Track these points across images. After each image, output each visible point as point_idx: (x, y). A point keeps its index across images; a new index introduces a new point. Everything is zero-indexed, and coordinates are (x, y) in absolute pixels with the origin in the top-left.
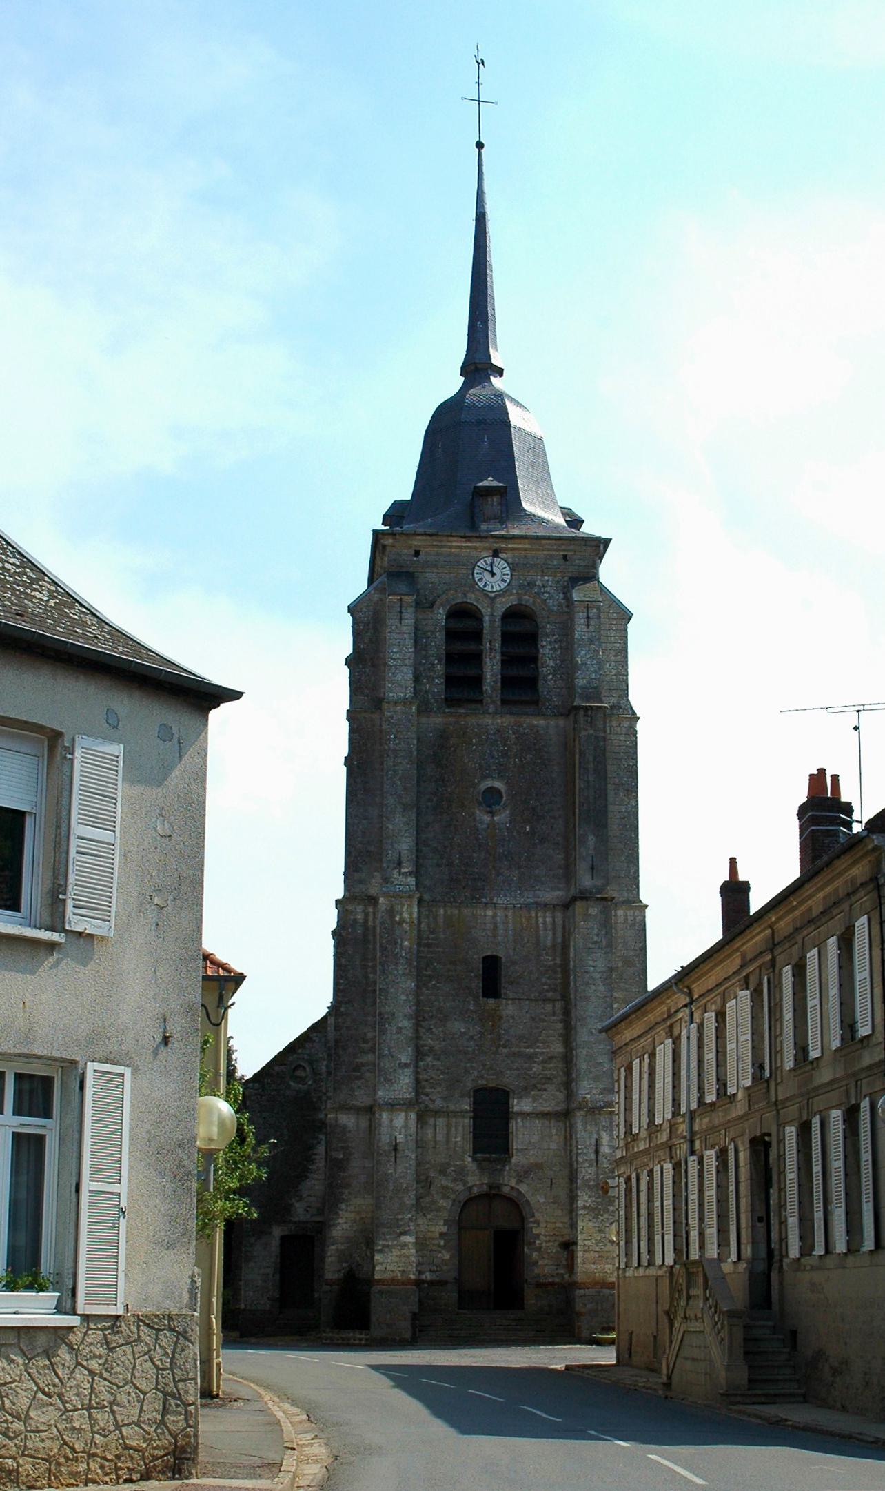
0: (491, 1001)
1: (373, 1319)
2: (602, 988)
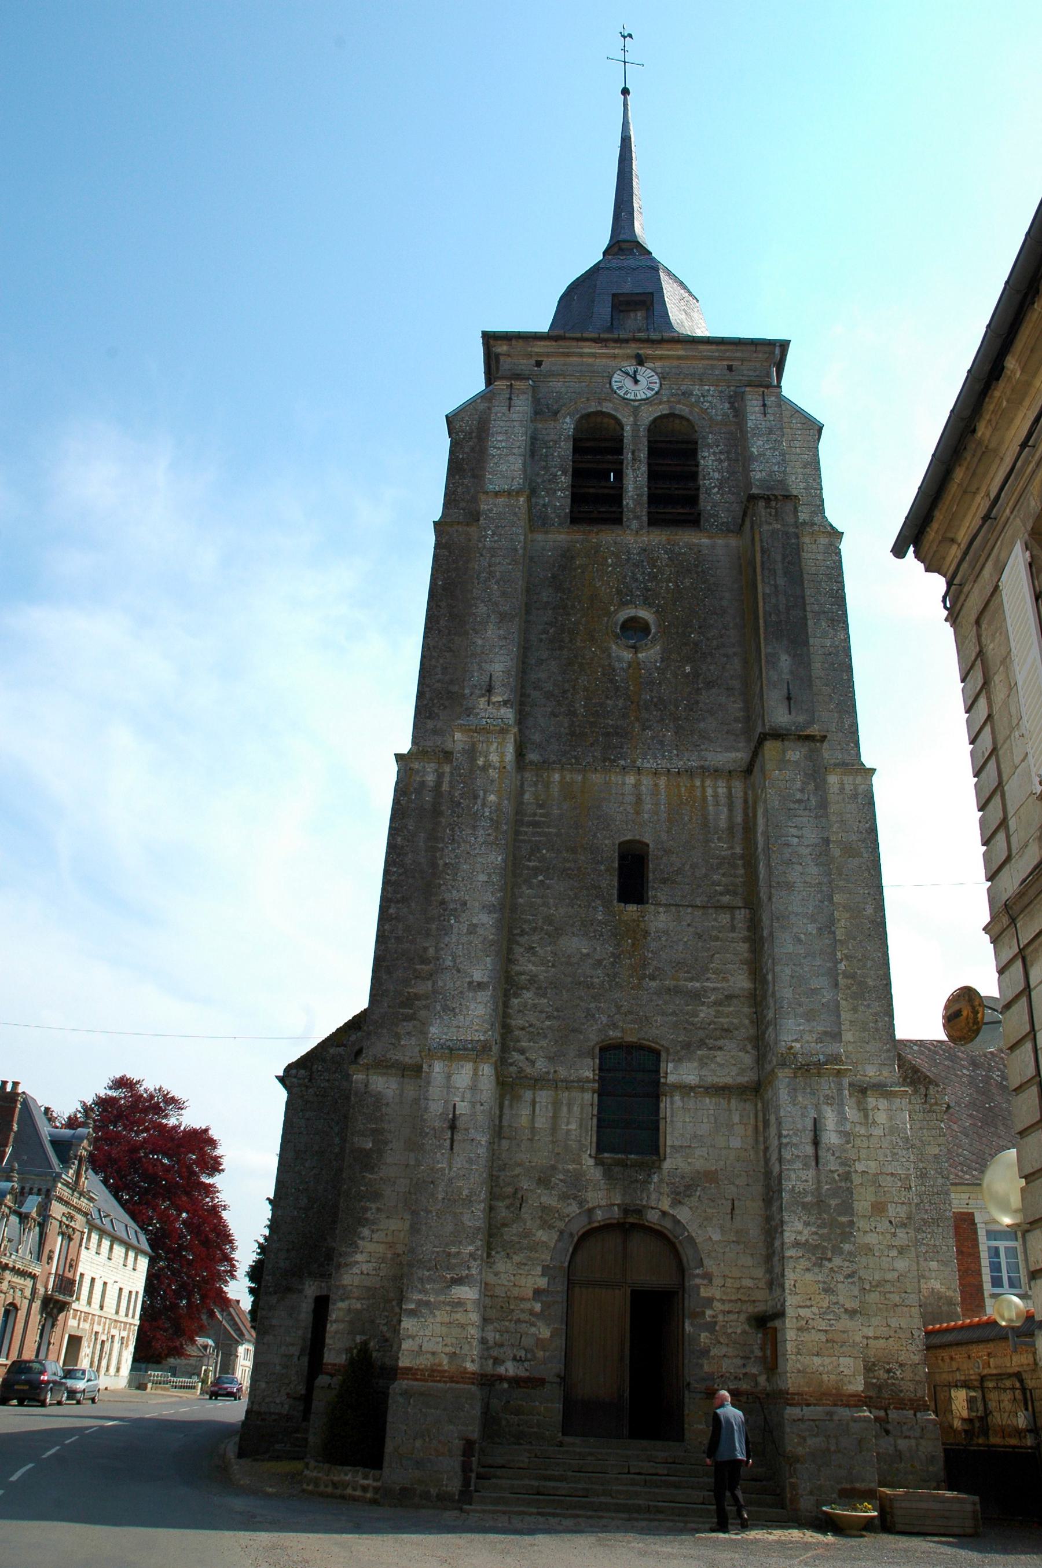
0: (632, 908)
1: (389, 1447)
2: (814, 870)
